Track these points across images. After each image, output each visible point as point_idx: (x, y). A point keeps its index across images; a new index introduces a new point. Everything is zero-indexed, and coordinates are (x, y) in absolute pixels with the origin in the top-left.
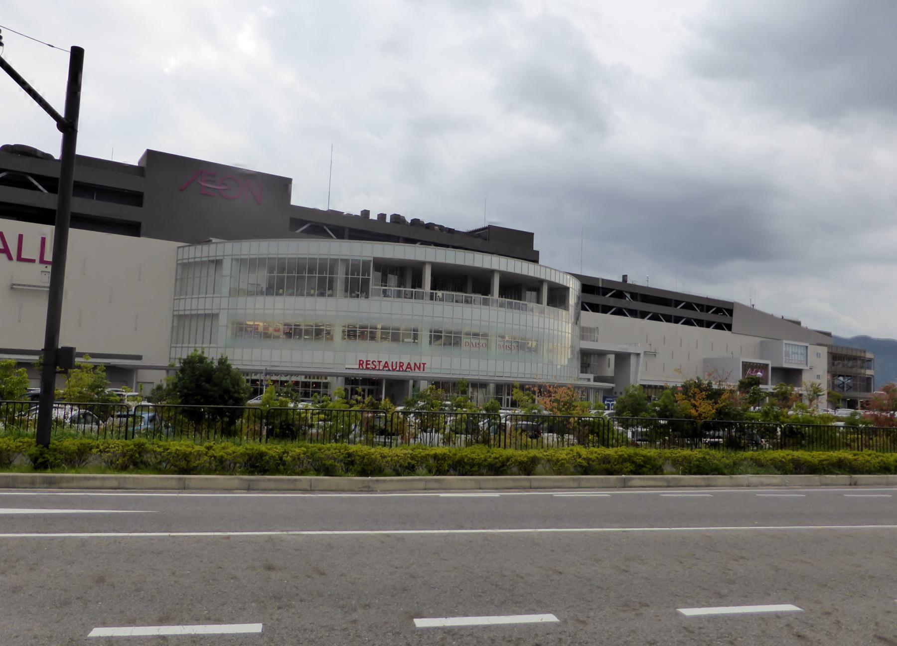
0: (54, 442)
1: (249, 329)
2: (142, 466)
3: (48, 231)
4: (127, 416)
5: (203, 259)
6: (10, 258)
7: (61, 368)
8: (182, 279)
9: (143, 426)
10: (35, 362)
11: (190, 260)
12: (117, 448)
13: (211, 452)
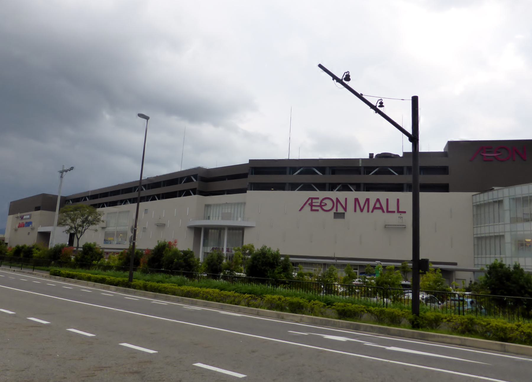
0: (421, 313)
1: (528, 244)
2: (473, 333)
3: (409, 195)
4: (455, 300)
5: (490, 201)
6: (383, 212)
7: (422, 271)
8: (477, 214)
9: (468, 307)
10: (400, 266)
11: (481, 203)
12: (457, 320)
13: (520, 329)
